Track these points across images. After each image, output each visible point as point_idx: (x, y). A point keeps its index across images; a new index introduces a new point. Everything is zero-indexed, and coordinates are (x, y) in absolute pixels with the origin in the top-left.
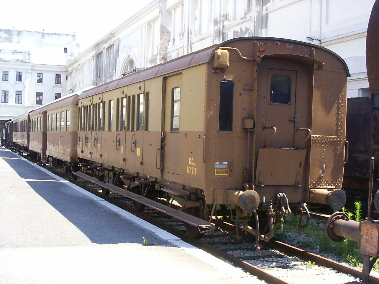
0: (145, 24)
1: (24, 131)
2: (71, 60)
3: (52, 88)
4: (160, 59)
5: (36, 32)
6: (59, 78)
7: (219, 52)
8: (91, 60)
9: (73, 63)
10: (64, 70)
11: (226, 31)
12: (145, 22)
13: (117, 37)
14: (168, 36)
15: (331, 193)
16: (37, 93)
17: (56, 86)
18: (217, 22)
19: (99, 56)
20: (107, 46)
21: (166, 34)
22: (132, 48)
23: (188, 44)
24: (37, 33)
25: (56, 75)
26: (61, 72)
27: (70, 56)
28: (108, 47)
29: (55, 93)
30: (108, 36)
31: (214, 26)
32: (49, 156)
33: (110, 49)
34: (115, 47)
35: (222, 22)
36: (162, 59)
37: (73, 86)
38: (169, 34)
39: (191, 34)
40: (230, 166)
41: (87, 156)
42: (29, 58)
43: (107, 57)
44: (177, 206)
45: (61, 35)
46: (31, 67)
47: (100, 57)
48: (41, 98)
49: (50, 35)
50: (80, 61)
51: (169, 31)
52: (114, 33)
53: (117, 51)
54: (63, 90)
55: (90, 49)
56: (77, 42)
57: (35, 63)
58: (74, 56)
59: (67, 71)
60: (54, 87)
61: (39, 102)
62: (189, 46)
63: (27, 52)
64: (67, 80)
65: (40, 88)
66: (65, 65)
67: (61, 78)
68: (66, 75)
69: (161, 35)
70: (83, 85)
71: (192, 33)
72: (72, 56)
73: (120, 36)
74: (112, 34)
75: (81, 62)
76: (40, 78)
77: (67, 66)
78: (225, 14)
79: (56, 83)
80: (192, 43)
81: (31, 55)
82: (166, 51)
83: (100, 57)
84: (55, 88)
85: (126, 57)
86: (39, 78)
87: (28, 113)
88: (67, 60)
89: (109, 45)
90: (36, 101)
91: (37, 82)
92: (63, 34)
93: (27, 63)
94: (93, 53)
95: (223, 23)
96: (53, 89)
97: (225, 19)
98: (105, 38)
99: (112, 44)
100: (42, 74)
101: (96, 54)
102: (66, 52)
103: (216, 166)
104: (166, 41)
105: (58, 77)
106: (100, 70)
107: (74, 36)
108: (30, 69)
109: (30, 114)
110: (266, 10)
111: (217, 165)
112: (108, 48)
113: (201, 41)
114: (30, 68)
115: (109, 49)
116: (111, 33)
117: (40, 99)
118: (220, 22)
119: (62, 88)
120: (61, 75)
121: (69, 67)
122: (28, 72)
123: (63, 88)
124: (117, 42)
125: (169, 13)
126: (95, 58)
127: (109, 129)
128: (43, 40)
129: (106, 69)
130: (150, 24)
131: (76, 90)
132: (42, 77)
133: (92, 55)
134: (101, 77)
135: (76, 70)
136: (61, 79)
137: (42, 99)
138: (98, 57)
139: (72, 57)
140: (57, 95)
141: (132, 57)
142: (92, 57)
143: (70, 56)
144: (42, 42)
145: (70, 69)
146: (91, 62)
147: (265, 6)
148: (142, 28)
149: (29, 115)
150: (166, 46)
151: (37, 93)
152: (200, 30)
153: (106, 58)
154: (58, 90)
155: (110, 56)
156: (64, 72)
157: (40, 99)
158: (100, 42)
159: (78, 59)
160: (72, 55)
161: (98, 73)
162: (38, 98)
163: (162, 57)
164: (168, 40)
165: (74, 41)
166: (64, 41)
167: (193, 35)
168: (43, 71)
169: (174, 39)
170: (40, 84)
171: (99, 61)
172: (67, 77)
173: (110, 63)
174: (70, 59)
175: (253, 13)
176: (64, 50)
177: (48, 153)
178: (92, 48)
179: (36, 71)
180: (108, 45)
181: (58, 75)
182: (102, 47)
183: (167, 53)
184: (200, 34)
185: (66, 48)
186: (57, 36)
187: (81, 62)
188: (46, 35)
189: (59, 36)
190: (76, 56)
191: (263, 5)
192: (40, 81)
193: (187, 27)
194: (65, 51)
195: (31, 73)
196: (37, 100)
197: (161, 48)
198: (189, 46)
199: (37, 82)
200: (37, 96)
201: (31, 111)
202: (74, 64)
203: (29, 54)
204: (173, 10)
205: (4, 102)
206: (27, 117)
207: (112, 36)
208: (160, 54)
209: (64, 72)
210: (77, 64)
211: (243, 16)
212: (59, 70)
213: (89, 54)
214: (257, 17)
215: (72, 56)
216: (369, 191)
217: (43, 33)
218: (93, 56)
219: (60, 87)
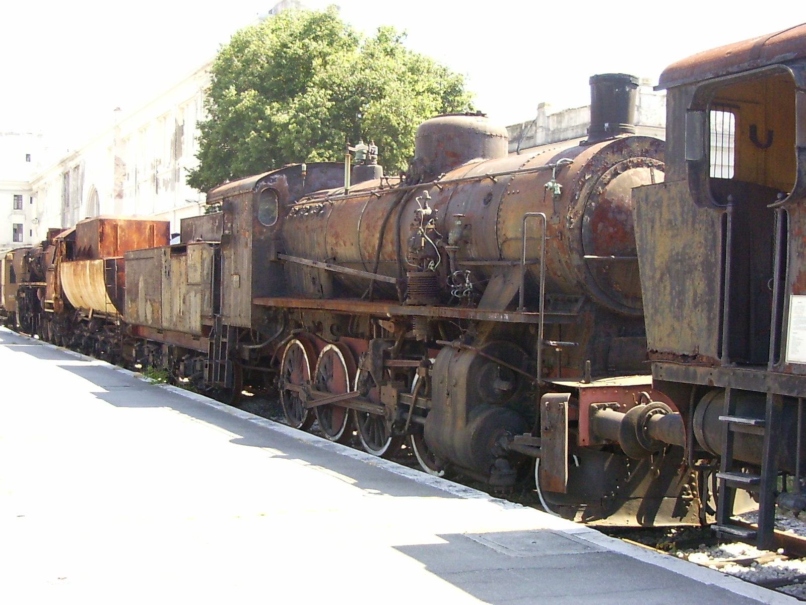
10: (27, 188)
14: (124, 169)
17: (15, 213)
18: (153, 167)
21: (121, 167)
26: (21, 191)
33: (78, 170)
34: (80, 168)
44: (627, 376)
59: (31, 190)
60: (12, 214)
64: (31, 203)
67: (21, 200)
69: (115, 168)
77: (30, 183)
78: (158, 159)
79: (14, 209)
82: (122, 187)
94: (61, 170)
102: (30, 161)
105: (18, 198)
110: (178, 164)
112: (75, 168)
121: (34, 185)
125: (124, 141)
136: (22, 203)
138: (65, 177)
145: (35, 187)
150: (122, 181)
154: (18, 220)
158: (65, 158)
163: (116, 194)
164: (124, 174)
169: (128, 174)
172: (31, 198)
175: (171, 167)
185: (29, 155)
202: (39, 181)
205: (254, 303)
212: (19, 188)
216: (114, 364)
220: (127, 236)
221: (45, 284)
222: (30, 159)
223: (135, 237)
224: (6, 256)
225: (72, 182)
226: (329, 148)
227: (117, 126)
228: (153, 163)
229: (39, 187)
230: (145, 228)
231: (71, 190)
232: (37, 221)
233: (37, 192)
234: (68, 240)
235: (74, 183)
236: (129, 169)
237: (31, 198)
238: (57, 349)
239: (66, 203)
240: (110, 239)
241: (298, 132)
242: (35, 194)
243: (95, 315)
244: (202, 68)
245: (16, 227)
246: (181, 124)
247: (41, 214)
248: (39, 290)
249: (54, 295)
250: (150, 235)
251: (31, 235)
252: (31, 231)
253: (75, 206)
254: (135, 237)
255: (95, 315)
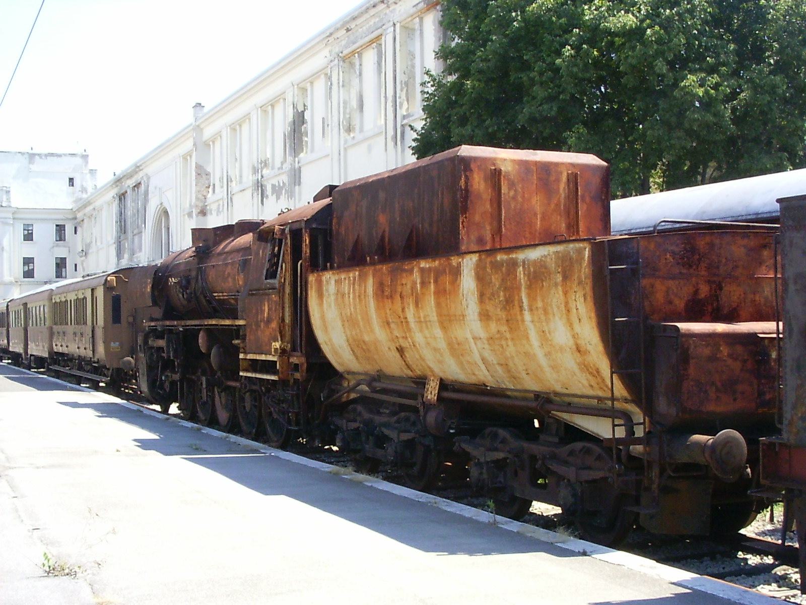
0: (180, 157)
1: (3, 327)
2: (81, 199)
3: (51, 249)
4: (197, 213)
5: (19, 152)
6: (61, 230)
7: (109, 278)
8: (112, 203)
9: (83, 205)
10: (71, 216)
11: (265, 183)
12: (179, 155)
13: (145, 171)
15: (711, 440)
16: (24, 258)
17: (57, 246)
18: (255, 170)
19: (123, 197)
20: (133, 184)
21: (204, 176)
22: (165, 191)
23: (228, 194)
24: (20, 154)
25: (57, 226)
27: (79, 191)
28: (134, 185)
29: (56, 258)
30: (133, 168)
31: (252, 175)
32: (31, 355)
33: (138, 188)
34: (143, 188)
35: (260, 171)
36: (200, 214)
37: (86, 245)
38: (208, 177)
39: (231, 181)
40: (121, 345)
41: (60, 350)
42: (7, 199)
43: (133, 201)
45: (63, 156)
46: (13, 214)
47: (124, 199)
48: (32, 267)
49: (43, 157)
50: (95, 202)
51: (209, 172)
52: (141, 166)
53: (146, 193)
54: (69, 252)
55: (108, 185)
56: (90, 167)
57: (19, 207)
58: (86, 192)
59: (75, 218)
60: (53, 247)
61: (29, 274)
62: (229, 198)
63: (5, 188)
64: (76, 233)
65: (28, 250)
66: (71, 208)
67: (65, 230)
68: (74, 224)
70: (102, 244)
71: (233, 179)
72: (83, 192)
73: (149, 170)
74: (138, 167)
75: (97, 204)
76: (28, 233)
77: (74, 210)
78: (263, 160)
79: (57, 241)
80: (232, 193)
81: (11, 192)
83: (124, 199)
84: (56, 249)
85: (158, 206)
86: (26, 232)
87: (6, 304)
88: (75, 199)
89: (135, 182)
90: (24, 272)
91: (24, 240)
92: (65, 155)
93: (6, 207)
94: (114, 192)
95: (261, 171)
96: (52, 250)
97: (263, 167)
98: (129, 171)
99: (139, 181)
100: (32, 225)
101: (118, 195)
102: (73, 185)
103: (111, 345)
104: (204, 187)
105: (60, 229)
106: (125, 221)
107: (85, 157)
108: (10, 218)
109: (9, 304)
110: (299, 163)
111: (112, 344)
112: (135, 186)
113: (241, 193)
114: (11, 216)
115: (136, 189)
116: (136, 164)
117: (30, 268)
118: (258, 170)
119: (68, 248)
120: (65, 225)
121: (79, 212)
122: (7, 224)
123: (69, 248)
124: (145, 179)
125: (207, 145)
126: (117, 201)
127: (71, 324)
128: (31, 166)
129: (133, 219)
130: (186, 157)
131: (90, 251)
132: (32, 230)
133: (112, 195)
134: (126, 232)
135: (89, 217)
136: (65, 233)
137: (33, 269)
138: (120, 199)
139: (84, 194)
140: (59, 261)
141: (166, 205)
142: (112, 198)
143: (79, 191)
144: (30, 169)
145: (79, 215)
146: (238, 131)
147: (298, 157)
148: (176, 162)
149: (8, 306)
150: (205, 194)
151: (24, 258)
152: (241, 176)
153: (133, 202)
154: (61, 252)
155: (138, 200)
156: (70, 219)
157: (30, 268)
159: (91, 199)
160: (84, 190)
161: (122, 225)
162: (27, 267)
165: (86, 166)
166: (67, 167)
167: (234, 183)
168: (31, 219)
169: (214, 185)
170: (28, 243)
171: (122, 205)
172: (76, 228)
173: (138, 211)
174: (79, 197)
175: (287, 166)
176: (69, 182)
177: (29, 353)
178: (110, 184)
179: (21, 221)
180: (134, 181)
181: (61, 225)
182: (125, 183)
183: (206, 204)
184: (241, 182)
186: (56, 157)
187: (97, 204)
188: (37, 157)
189: (59, 158)
190: (90, 190)
191: (295, 157)
192: (29, 237)
193: (226, 171)
194: (71, 183)
195: (13, 224)
196: (25, 270)
197: (197, 199)
198: (229, 198)
199: (24, 240)
200: (24, 264)
201: (11, 301)
202: (85, 208)
203: (8, 192)
204: (211, 143)
206: (5, 308)
207: (137, 170)
208: (197, 206)
209: (70, 219)
210: (91, 208)
211: (279, 165)
212: (61, 217)
213: (108, 192)
214: (291, 169)
215: (83, 192)
217: (31, 154)
218: (113, 197)
219: (65, 246)
220: (520, 199)
221: (241, 322)
222: (73, 183)
223: (537, 203)
224: (106, 280)
225: (129, 203)
226: (712, 70)
227: (198, 126)
228: (256, 165)
229: (85, 214)
230: (558, 180)
231: (129, 213)
232: (84, 253)
233: (83, 220)
234: (314, 226)
235: (133, 204)
236: (216, 178)
237: (76, 228)
238: (192, 427)
239: (121, 229)
240: (482, 208)
241: (659, 41)
242: (79, 223)
243: (446, 394)
244: (343, 26)
245: (58, 262)
246: (300, 109)
247: (88, 245)
248: (201, 335)
249: (277, 345)
250: (568, 197)
251: (76, 270)
252: (76, 265)
253: (135, 233)
254: (537, 203)
255: (446, 394)
